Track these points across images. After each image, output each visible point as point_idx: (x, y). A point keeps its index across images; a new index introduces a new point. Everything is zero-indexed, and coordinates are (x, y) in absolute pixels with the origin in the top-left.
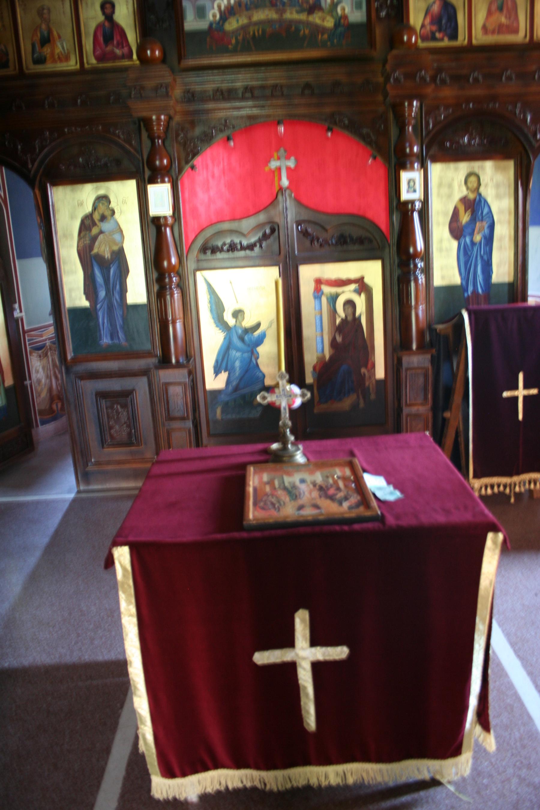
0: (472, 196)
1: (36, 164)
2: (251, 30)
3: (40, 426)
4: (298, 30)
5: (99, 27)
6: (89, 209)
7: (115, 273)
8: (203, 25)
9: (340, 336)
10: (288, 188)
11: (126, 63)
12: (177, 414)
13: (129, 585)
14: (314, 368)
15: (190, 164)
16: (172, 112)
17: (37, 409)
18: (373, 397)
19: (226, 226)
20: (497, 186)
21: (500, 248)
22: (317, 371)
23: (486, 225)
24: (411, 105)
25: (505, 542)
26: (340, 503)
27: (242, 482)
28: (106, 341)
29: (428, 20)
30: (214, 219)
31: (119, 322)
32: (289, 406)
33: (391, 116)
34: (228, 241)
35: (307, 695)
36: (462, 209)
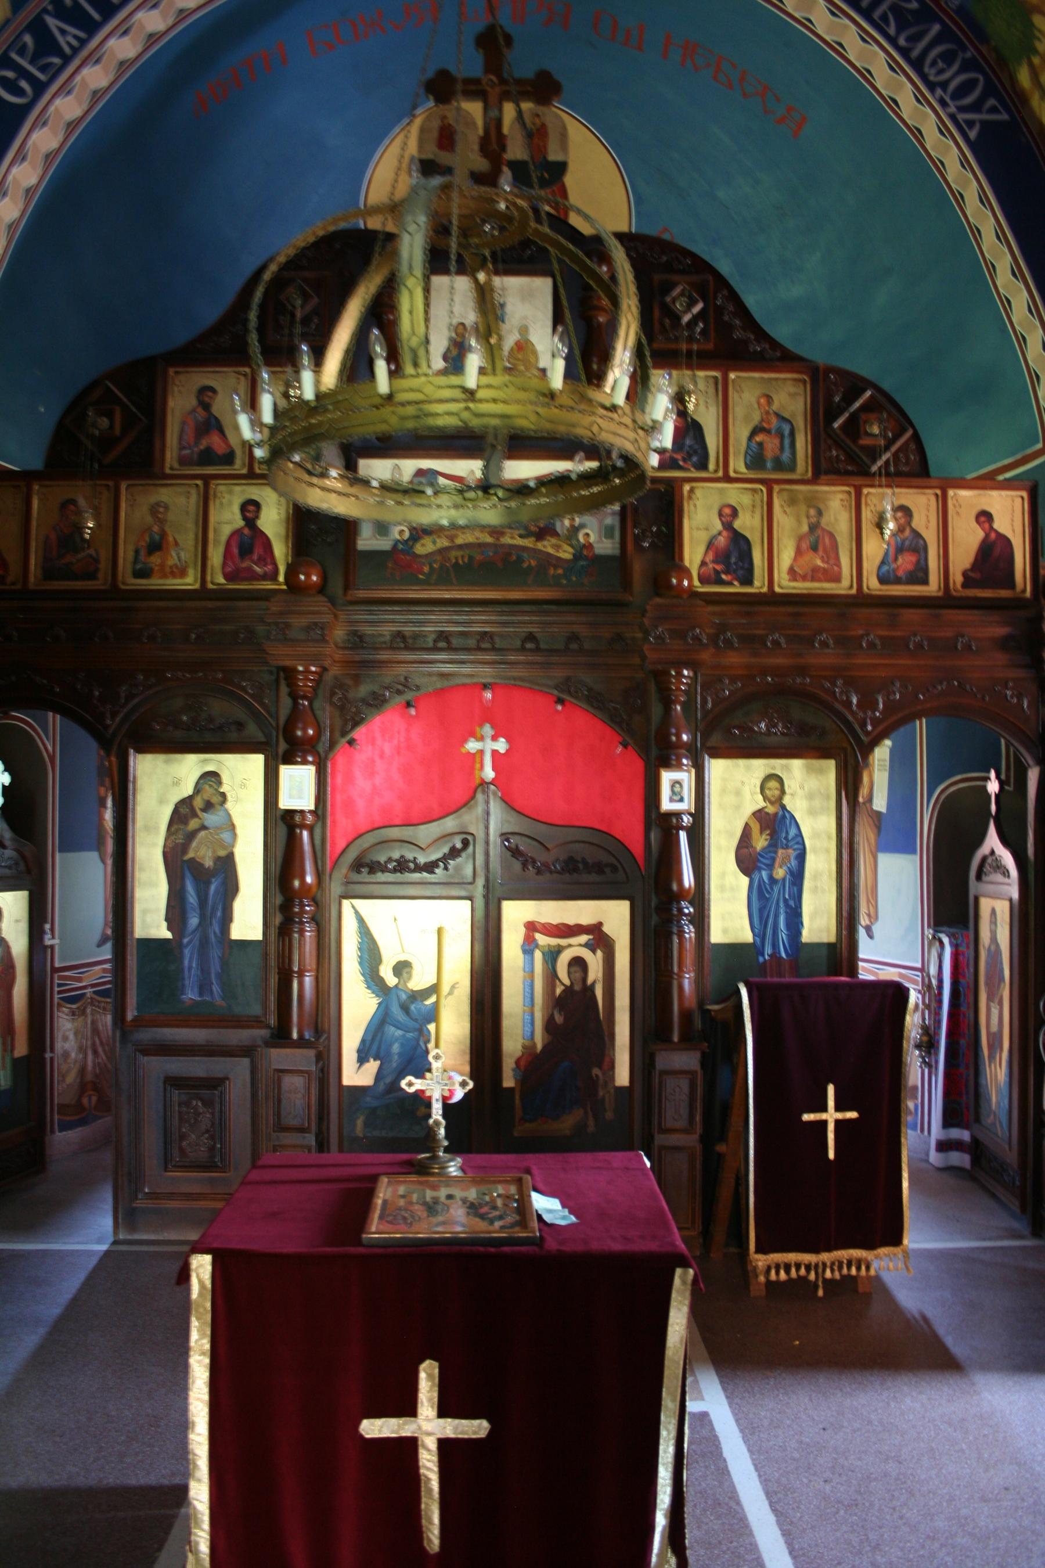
0: (771, 809)
1: (118, 719)
2: (453, 554)
3: (57, 1133)
4: (520, 560)
5: (236, 533)
6: (188, 790)
7: (216, 891)
8: (384, 544)
9: (561, 1014)
10: (493, 782)
11: (269, 586)
12: (294, 1122)
13: (205, 1309)
14: (518, 1062)
15: (348, 738)
16: (327, 663)
17: (56, 1102)
18: (609, 1115)
19: (394, 833)
20: (810, 797)
21: (815, 890)
22: (522, 1068)
23: (792, 853)
24: (680, 674)
25: (695, 1282)
26: (491, 1222)
27: (369, 1194)
28: (191, 995)
29: (710, 557)
30: (378, 820)
31: (215, 967)
32: (445, 1099)
33: (652, 688)
34: (396, 855)
35: (430, 1491)
36: (755, 827)
